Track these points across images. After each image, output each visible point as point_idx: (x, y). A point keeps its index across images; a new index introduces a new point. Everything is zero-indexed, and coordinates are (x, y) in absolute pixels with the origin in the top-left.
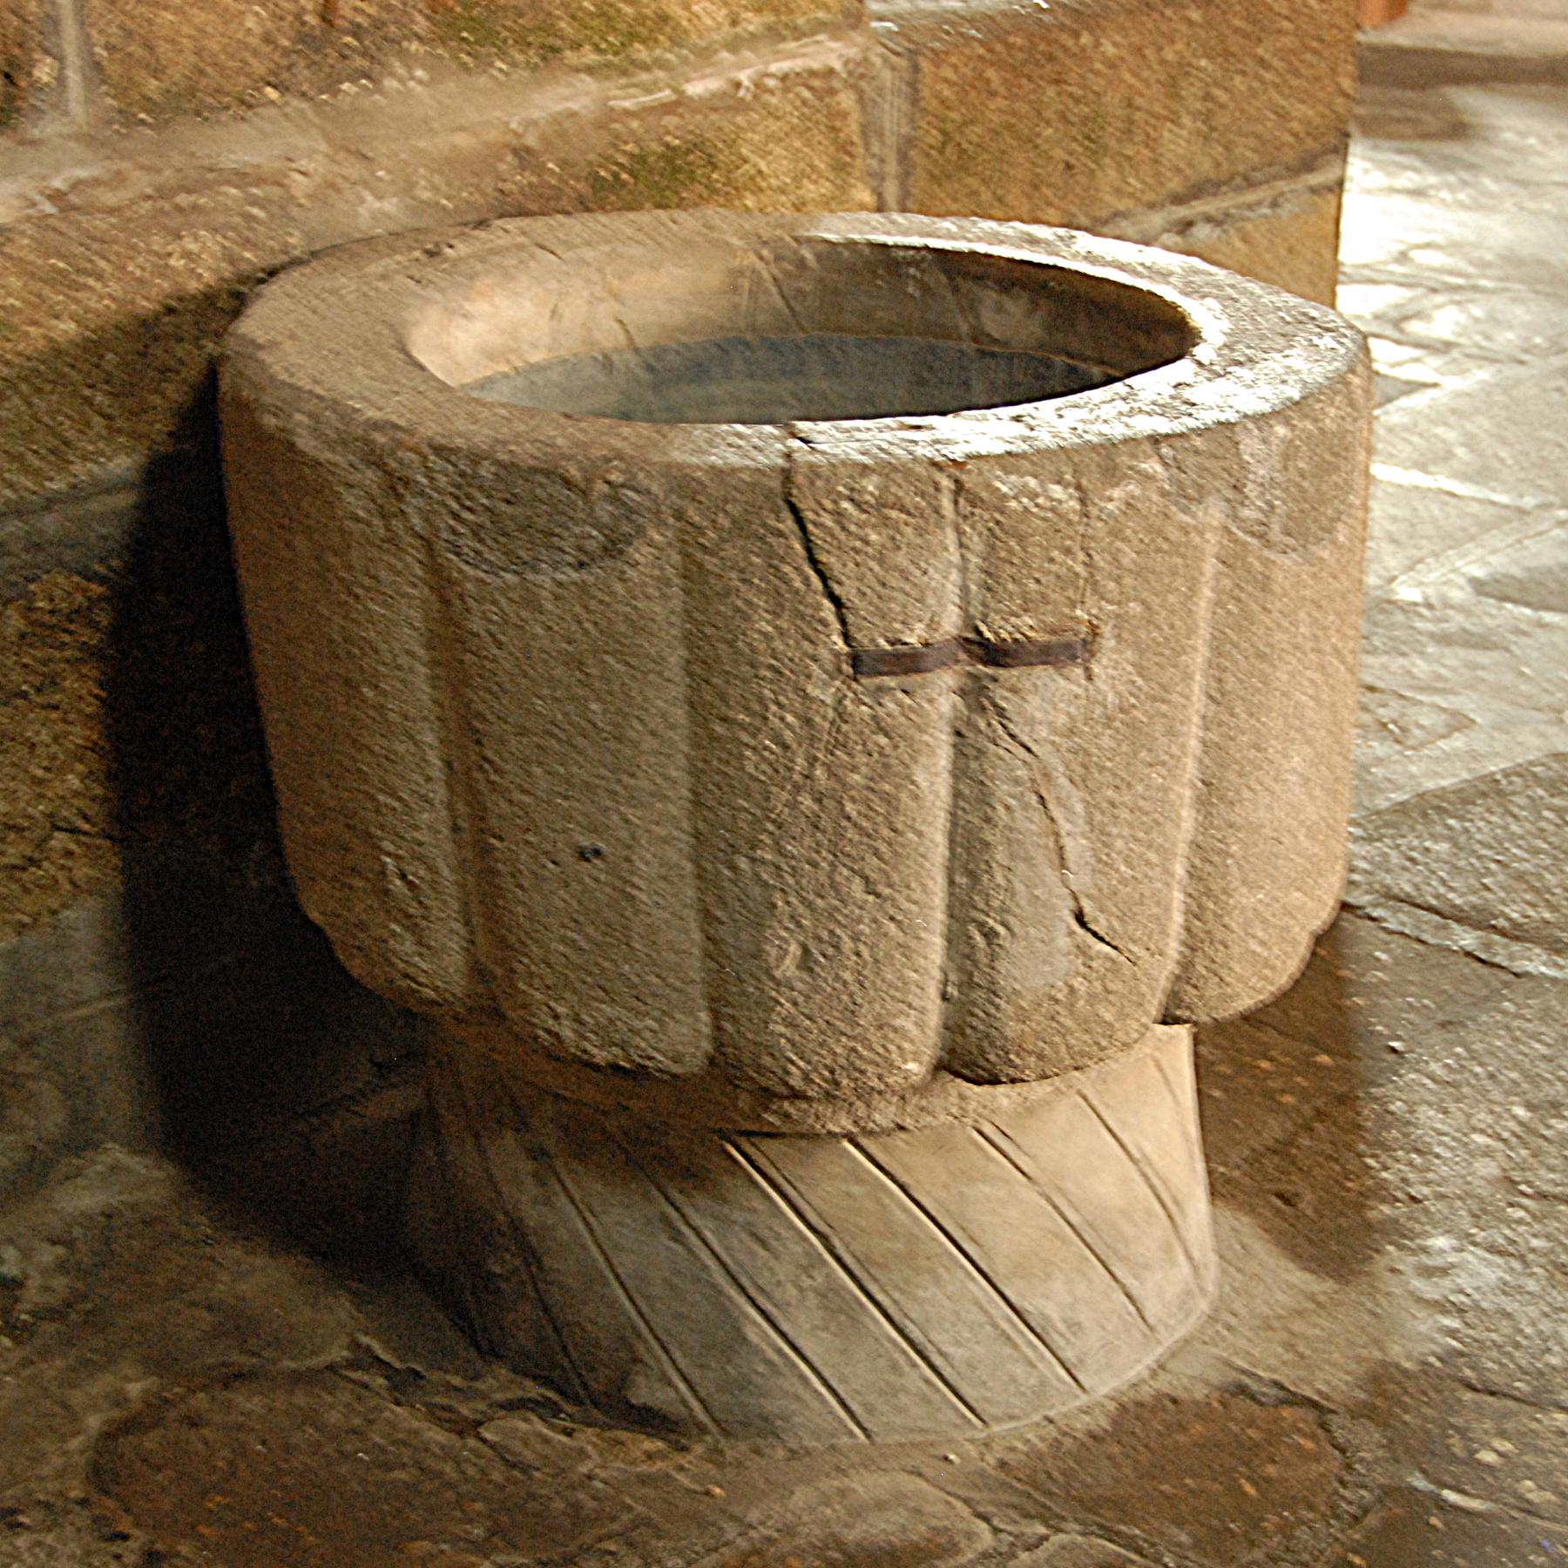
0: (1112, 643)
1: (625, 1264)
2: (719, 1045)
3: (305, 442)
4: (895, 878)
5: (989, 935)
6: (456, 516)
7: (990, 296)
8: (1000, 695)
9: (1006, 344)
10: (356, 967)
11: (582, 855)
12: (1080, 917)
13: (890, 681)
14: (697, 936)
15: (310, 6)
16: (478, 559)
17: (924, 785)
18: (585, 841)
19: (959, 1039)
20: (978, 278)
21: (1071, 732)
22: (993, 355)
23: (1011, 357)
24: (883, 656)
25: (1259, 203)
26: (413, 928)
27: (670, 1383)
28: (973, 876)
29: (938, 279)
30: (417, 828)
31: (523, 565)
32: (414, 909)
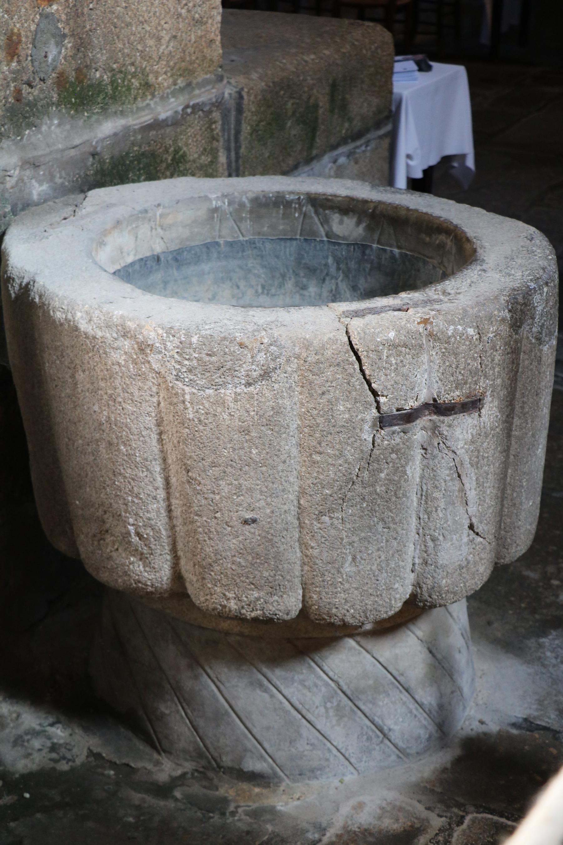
0: (490, 399)
1: (239, 705)
2: (304, 606)
3: (83, 326)
4: (397, 519)
5: (434, 540)
6: (179, 363)
7: (336, 217)
8: (444, 429)
9: (344, 238)
10: (104, 577)
11: (246, 522)
12: (471, 527)
13: (396, 428)
14: (299, 554)
15: (3, 93)
16: (192, 383)
17: (410, 475)
18: (248, 516)
19: (418, 590)
20: (332, 208)
21: (472, 442)
22: (339, 244)
23: (348, 245)
24: (394, 417)
25: (361, 146)
26: (142, 557)
27: (265, 760)
28: (429, 514)
29: (309, 209)
30: (148, 512)
31: (217, 386)
32: (145, 550)
